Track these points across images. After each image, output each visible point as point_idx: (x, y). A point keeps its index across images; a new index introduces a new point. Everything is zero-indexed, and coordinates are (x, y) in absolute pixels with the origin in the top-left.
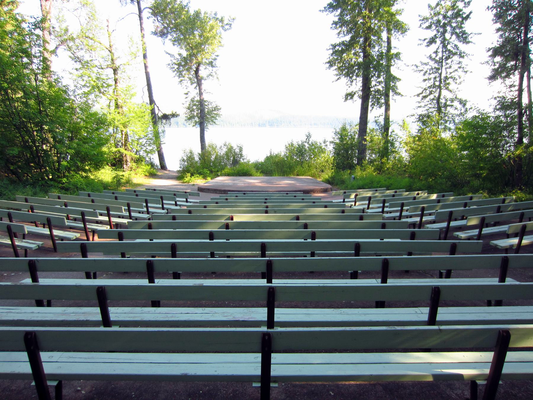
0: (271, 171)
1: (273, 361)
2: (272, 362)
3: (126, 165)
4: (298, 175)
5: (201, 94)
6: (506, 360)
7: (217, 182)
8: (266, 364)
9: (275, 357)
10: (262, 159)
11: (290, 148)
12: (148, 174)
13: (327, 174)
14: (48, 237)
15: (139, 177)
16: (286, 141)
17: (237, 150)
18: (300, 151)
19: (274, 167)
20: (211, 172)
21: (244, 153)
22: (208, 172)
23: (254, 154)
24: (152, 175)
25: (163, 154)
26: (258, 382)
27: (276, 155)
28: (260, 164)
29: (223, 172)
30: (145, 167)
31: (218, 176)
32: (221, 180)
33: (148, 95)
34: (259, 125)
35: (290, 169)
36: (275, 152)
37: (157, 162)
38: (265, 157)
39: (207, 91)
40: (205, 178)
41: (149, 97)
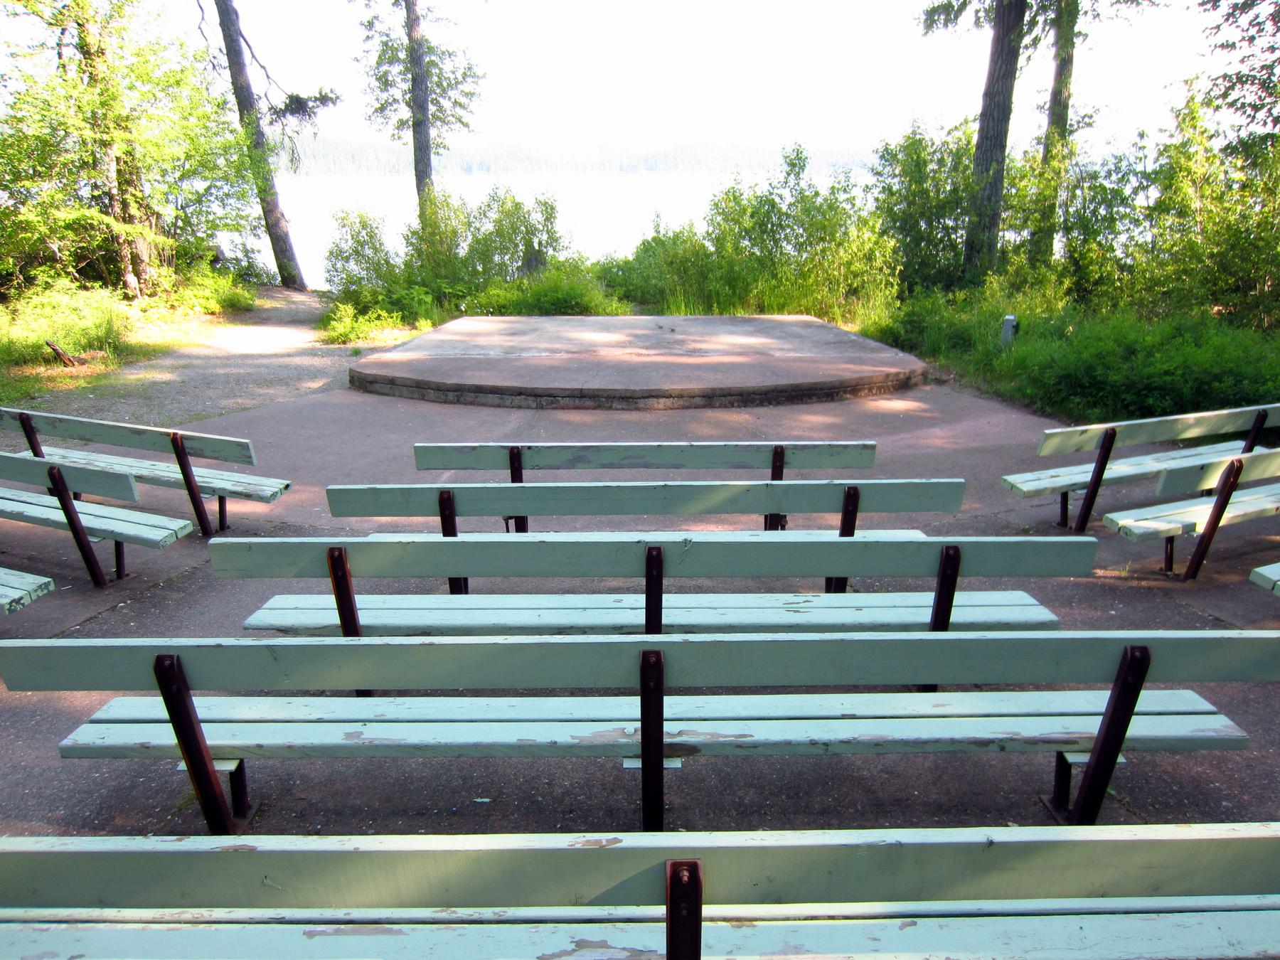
0: (662, 291)
1: (664, 604)
2: (666, 714)
3: (138, 274)
4: (761, 309)
5: (412, 22)
6: (1137, 709)
7: (453, 344)
8: (652, 718)
9: (672, 705)
10: (625, 250)
11: (730, 209)
12: (216, 308)
13: (878, 309)
14: (199, 454)
15: (177, 322)
16: (713, 186)
17: (537, 218)
18: (764, 219)
19: (668, 281)
20: (440, 298)
21: (560, 226)
22: (429, 299)
23: (596, 236)
24: (236, 311)
25: (287, 235)
26: (636, 757)
27: (677, 236)
28: (619, 267)
29: (482, 298)
30: (211, 287)
31: (459, 314)
32: (477, 336)
33: (217, 20)
34: (621, 169)
35: (733, 287)
36: (672, 225)
37: (267, 260)
38: (638, 242)
39: (437, 14)
40: (410, 318)
41: (222, 24)
